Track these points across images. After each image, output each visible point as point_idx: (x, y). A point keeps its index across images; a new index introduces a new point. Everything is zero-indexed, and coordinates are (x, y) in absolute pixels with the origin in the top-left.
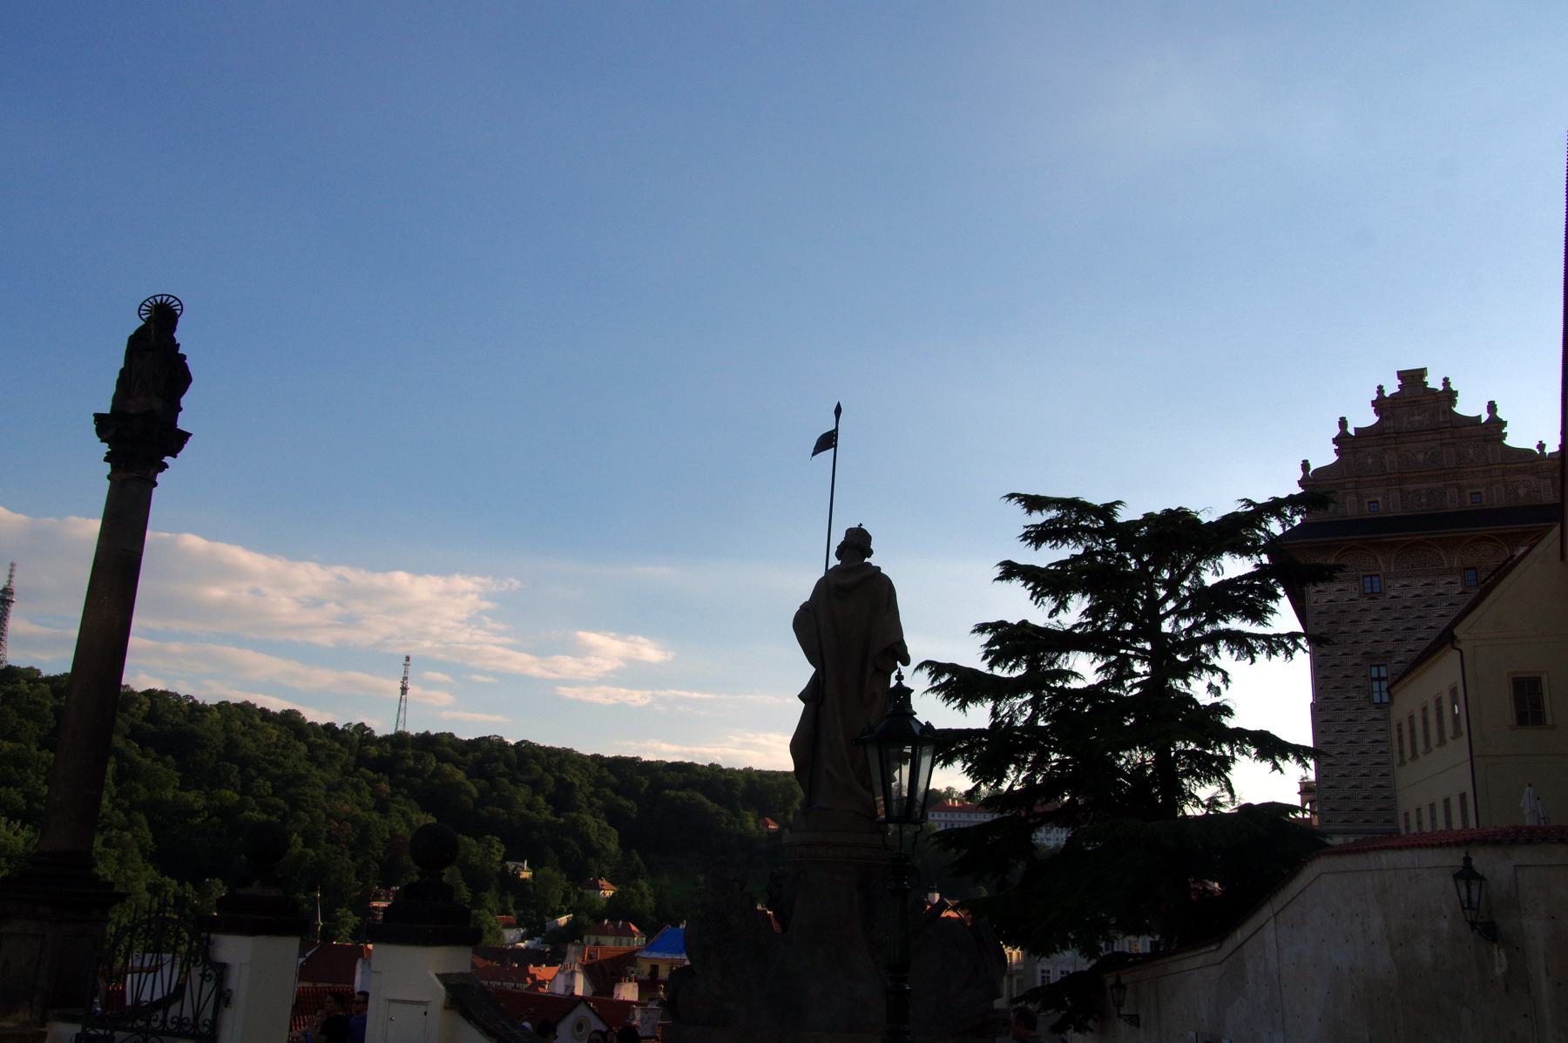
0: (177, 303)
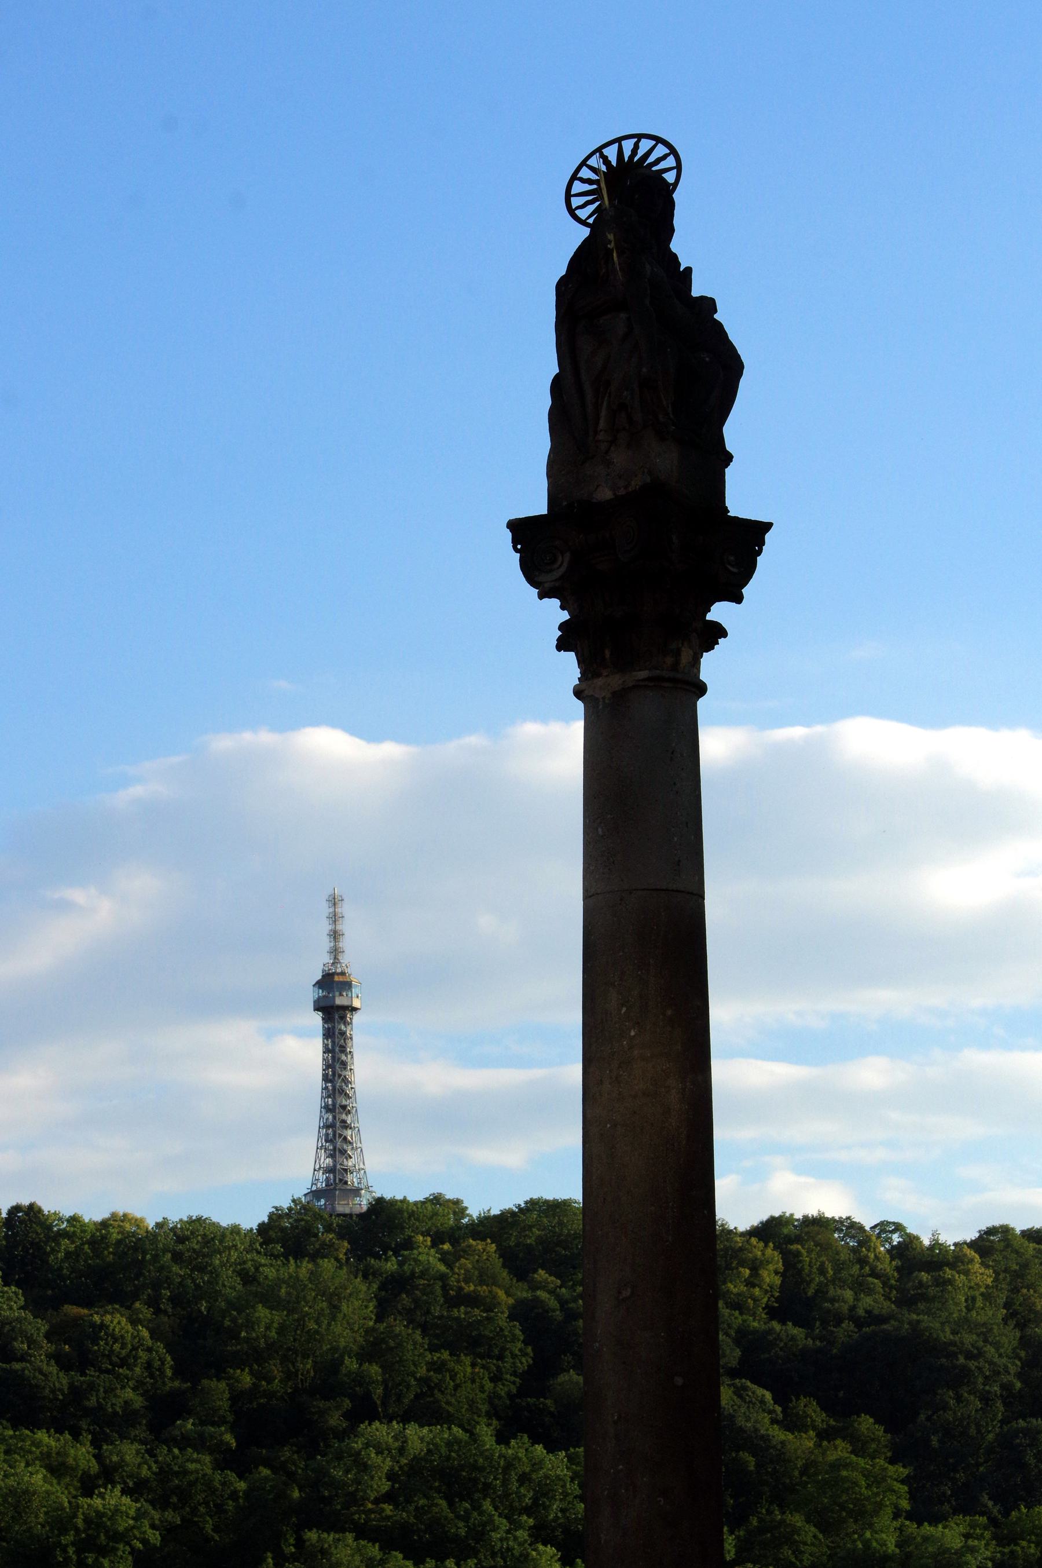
0: (661, 150)
